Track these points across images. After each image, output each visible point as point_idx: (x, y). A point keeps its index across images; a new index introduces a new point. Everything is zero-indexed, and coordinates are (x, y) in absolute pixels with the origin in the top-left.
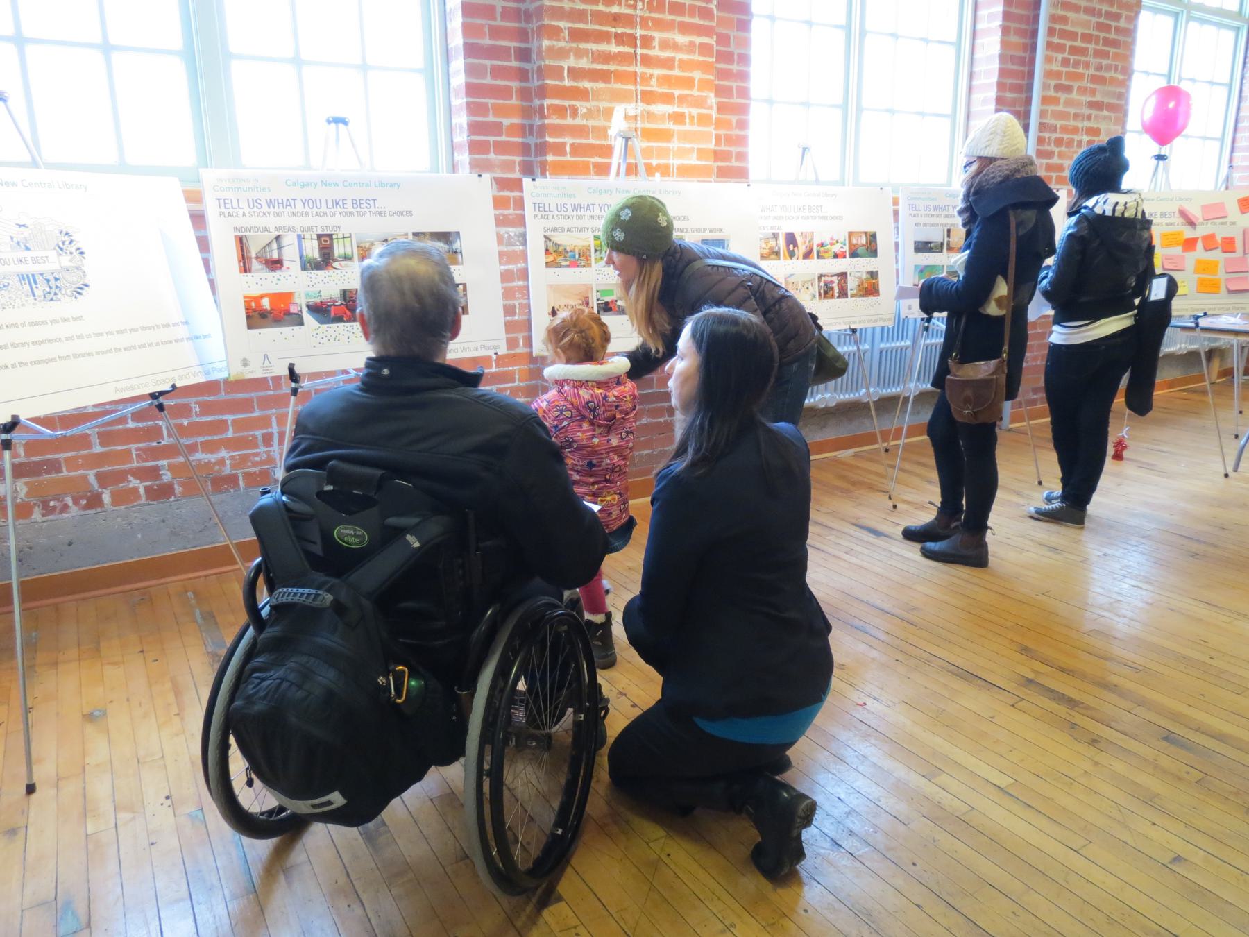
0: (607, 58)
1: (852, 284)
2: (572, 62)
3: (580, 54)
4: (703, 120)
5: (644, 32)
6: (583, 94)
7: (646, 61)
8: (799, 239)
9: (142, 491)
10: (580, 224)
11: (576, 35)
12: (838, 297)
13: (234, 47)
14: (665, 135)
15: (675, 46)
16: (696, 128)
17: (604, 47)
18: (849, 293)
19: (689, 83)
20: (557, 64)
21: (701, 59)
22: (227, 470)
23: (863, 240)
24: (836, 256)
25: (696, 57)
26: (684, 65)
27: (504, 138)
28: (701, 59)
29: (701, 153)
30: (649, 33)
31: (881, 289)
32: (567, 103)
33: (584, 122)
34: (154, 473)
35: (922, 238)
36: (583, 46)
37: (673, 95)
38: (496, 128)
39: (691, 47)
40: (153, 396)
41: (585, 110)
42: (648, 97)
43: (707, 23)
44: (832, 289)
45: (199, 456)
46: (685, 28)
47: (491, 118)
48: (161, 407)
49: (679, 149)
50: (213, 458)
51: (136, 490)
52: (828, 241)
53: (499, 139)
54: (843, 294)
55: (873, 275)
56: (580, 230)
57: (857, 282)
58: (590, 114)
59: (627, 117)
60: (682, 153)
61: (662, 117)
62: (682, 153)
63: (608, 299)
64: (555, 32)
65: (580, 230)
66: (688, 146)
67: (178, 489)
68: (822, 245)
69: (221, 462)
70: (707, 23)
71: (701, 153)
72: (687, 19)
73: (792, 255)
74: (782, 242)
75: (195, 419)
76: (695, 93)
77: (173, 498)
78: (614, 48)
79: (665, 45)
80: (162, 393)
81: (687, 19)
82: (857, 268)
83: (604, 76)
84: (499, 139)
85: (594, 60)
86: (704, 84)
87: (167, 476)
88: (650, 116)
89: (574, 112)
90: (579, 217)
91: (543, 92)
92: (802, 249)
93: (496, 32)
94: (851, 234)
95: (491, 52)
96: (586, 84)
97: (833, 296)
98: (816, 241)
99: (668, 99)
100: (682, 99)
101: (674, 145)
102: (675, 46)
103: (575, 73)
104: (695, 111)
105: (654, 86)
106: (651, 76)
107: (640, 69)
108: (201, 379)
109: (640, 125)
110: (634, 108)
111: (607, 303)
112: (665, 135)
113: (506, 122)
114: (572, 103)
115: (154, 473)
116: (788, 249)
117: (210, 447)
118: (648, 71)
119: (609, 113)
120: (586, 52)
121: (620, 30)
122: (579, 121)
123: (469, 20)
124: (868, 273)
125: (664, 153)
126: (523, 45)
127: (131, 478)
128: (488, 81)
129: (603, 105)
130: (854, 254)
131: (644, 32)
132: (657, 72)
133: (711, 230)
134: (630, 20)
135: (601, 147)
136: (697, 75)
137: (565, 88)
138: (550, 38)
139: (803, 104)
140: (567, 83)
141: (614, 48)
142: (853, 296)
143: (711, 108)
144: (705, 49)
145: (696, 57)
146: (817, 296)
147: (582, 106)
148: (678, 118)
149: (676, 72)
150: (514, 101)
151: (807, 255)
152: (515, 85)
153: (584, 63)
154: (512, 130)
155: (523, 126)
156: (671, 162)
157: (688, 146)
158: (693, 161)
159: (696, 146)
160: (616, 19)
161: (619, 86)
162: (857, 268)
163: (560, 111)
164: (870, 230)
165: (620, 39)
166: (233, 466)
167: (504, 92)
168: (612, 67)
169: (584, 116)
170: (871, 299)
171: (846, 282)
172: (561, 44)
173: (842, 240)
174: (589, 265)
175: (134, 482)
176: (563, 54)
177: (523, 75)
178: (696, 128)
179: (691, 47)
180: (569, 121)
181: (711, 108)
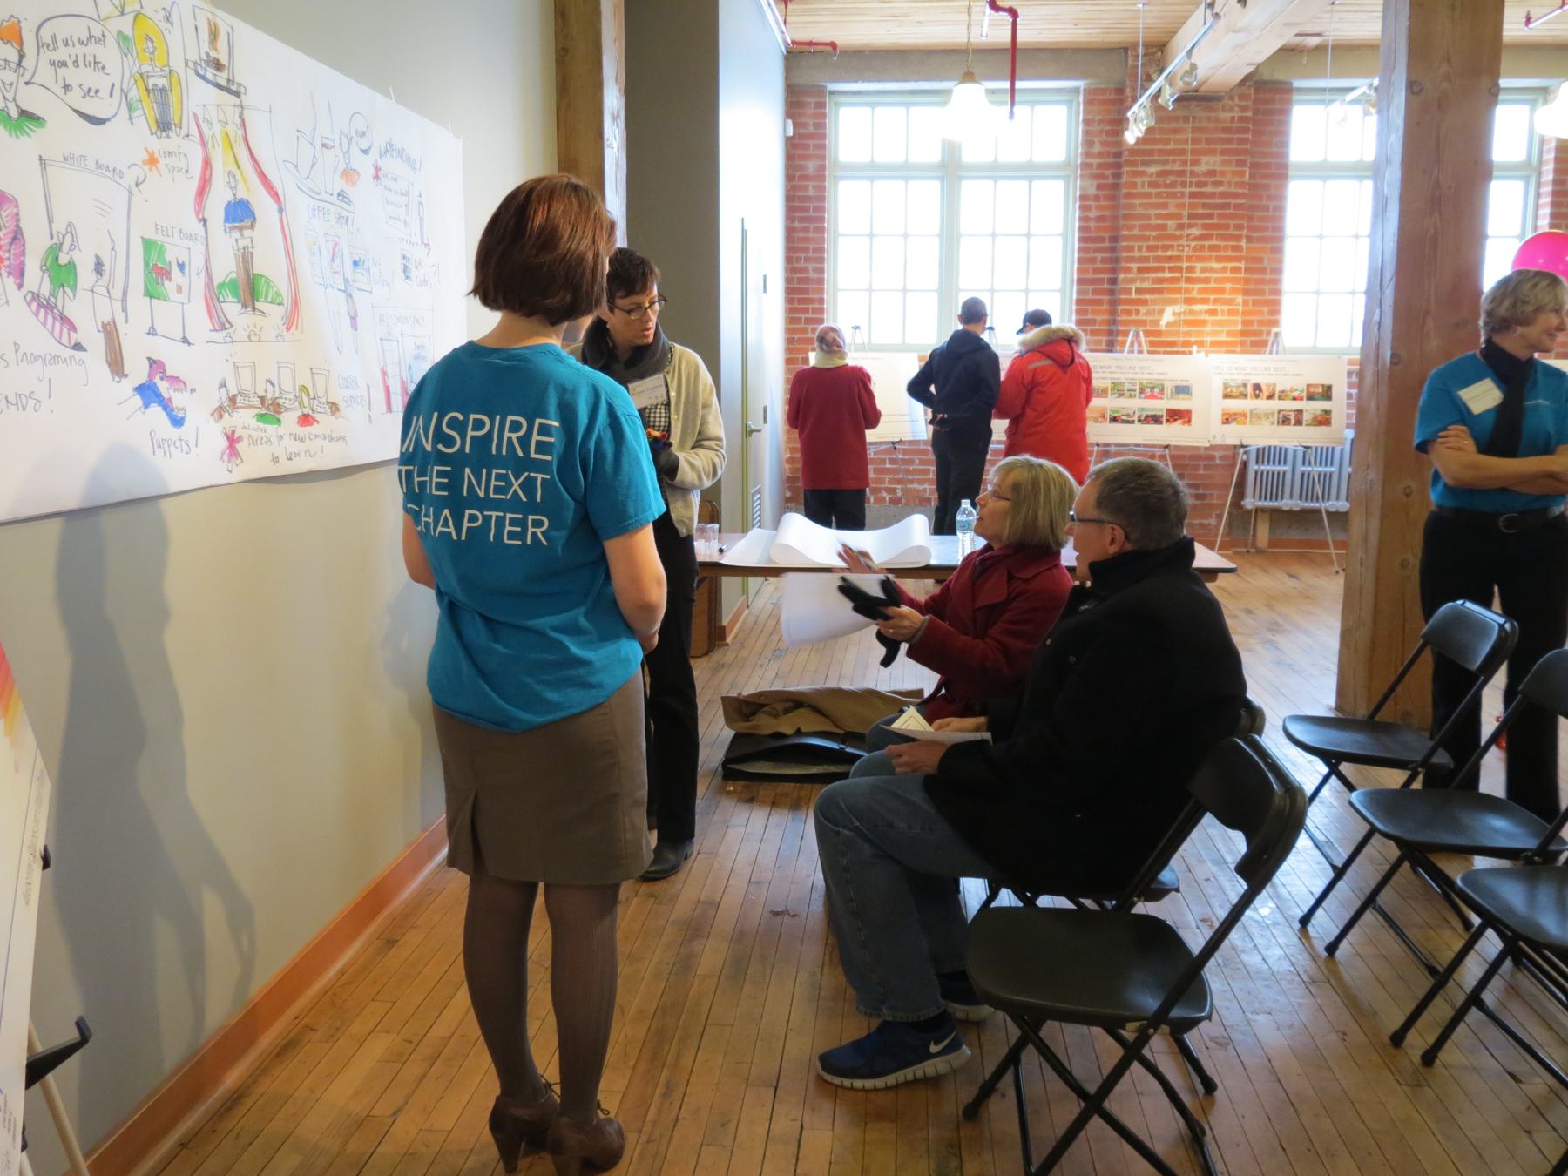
0: (1161, 281)
1: (1306, 417)
2: (1139, 285)
3: (1143, 280)
4: (1231, 312)
5: (1188, 264)
6: (1144, 302)
7: (1189, 280)
8: (1264, 388)
9: (887, 499)
10: (1104, 375)
11: (1140, 270)
12: (1295, 425)
13: (961, 287)
14: (1203, 323)
15: (1212, 270)
16: (1225, 318)
17: (1160, 275)
18: (1304, 423)
19: (1222, 291)
20: (1128, 286)
21: (1232, 276)
22: (927, 495)
23: (1320, 390)
24: (1295, 399)
25: (1228, 275)
26: (1217, 280)
27: (1097, 327)
28: (1232, 276)
29: (1229, 333)
30: (1192, 264)
31: (1333, 421)
32: (1133, 308)
33: (1144, 318)
34: (894, 490)
35: (105, 370)
36: (1146, 275)
37: (1209, 299)
38: (1093, 322)
39: (1224, 270)
40: (893, 443)
41: (1145, 311)
42: (1189, 301)
43: (1238, 254)
44: (1289, 419)
45: (915, 486)
46: (1219, 259)
47: (1090, 316)
48: (895, 448)
49: (1212, 331)
50: (921, 487)
51: (885, 498)
52: (1288, 389)
53: (1094, 328)
54: (1299, 422)
55: (1327, 412)
56: (1104, 378)
57: (1311, 416)
58: (1148, 313)
59: (1174, 314)
60: (1213, 333)
61: (1200, 312)
62: (1213, 333)
63: (1116, 415)
64: (1128, 270)
65: (1104, 378)
66: (1219, 329)
67: (903, 501)
68: (1283, 392)
69: (925, 490)
70: (1238, 254)
71: (1229, 333)
72: (1222, 254)
73: (1257, 396)
74: (1137, 388)
75: (916, 467)
76: (1227, 296)
77: (900, 505)
78: (1167, 275)
79: (1203, 270)
80: (896, 442)
81: (1222, 254)
82: (1313, 408)
83: (1160, 291)
84: (1094, 328)
85: (1153, 283)
86: (1233, 291)
87: (899, 493)
88: (1192, 312)
89: (1138, 312)
90: (1104, 372)
91: (1120, 302)
92: (1266, 393)
93: (1096, 271)
94: (1308, 386)
95: (1092, 282)
96: (1148, 297)
97: (1289, 424)
98: (1278, 389)
99: (1205, 301)
100: (1216, 301)
101: (1208, 328)
102: (1212, 270)
103: (1139, 291)
104: (1226, 308)
105: (1195, 295)
106: (1193, 289)
107: (1184, 285)
108: (911, 439)
109: (1182, 317)
110: (1178, 308)
111: (1115, 417)
112: (1203, 323)
113: (1098, 318)
114: (1136, 307)
115: (894, 490)
116: (1255, 393)
117: (920, 482)
118: (1191, 286)
119: (1161, 312)
120: (1148, 278)
121: (1172, 265)
122: (1141, 317)
123: (1082, 266)
124: (1323, 411)
125: (1202, 333)
126: (1112, 276)
127: (884, 492)
128: (1090, 296)
129: (1157, 308)
130: (1311, 397)
131: (1188, 264)
132: (1197, 286)
133: (1182, 381)
134: (1179, 259)
135: (1156, 331)
136: (1228, 286)
137: (1133, 300)
138: (1125, 273)
139: (1350, 293)
140: (1134, 296)
141: (1167, 275)
142: (1307, 425)
143: (1238, 304)
144: (1235, 270)
145: (1228, 275)
146: (1276, 422)
147: (1143, 309)
148: (1213, 312)
149: (1212, 285)
150: (1105, 307)
151: (1270, 397)
152: (1106, 298)
153: (1146, 285)
154: (1102, 322)
155: (1109, 321)
156: (1206, 339)
157: (1219, 329)
158: (1223, 338)
159: (1225, 329)
160: (1170, 258)
161: (1170, 296)
162: (1313, 408)
163: (1129, 312)
164: (1327, 383)
165: (1171, 269)
166: (930, 494)
167: (1099, 302)
168: (1164, 286)
169: (1144, 314)
170: (1323, 428)
171: (1302, 416)
172: (1133, 276)
173: (1301, 388)
174: (1107, 397)
175: (884, 494)
176: (1133, 281)
177: (1112, 292)
178: (1225, 318)
179: (1224, 270)
180: (1134, 317)
181: (1238, 304)
